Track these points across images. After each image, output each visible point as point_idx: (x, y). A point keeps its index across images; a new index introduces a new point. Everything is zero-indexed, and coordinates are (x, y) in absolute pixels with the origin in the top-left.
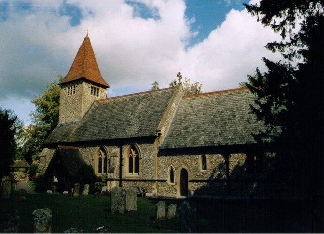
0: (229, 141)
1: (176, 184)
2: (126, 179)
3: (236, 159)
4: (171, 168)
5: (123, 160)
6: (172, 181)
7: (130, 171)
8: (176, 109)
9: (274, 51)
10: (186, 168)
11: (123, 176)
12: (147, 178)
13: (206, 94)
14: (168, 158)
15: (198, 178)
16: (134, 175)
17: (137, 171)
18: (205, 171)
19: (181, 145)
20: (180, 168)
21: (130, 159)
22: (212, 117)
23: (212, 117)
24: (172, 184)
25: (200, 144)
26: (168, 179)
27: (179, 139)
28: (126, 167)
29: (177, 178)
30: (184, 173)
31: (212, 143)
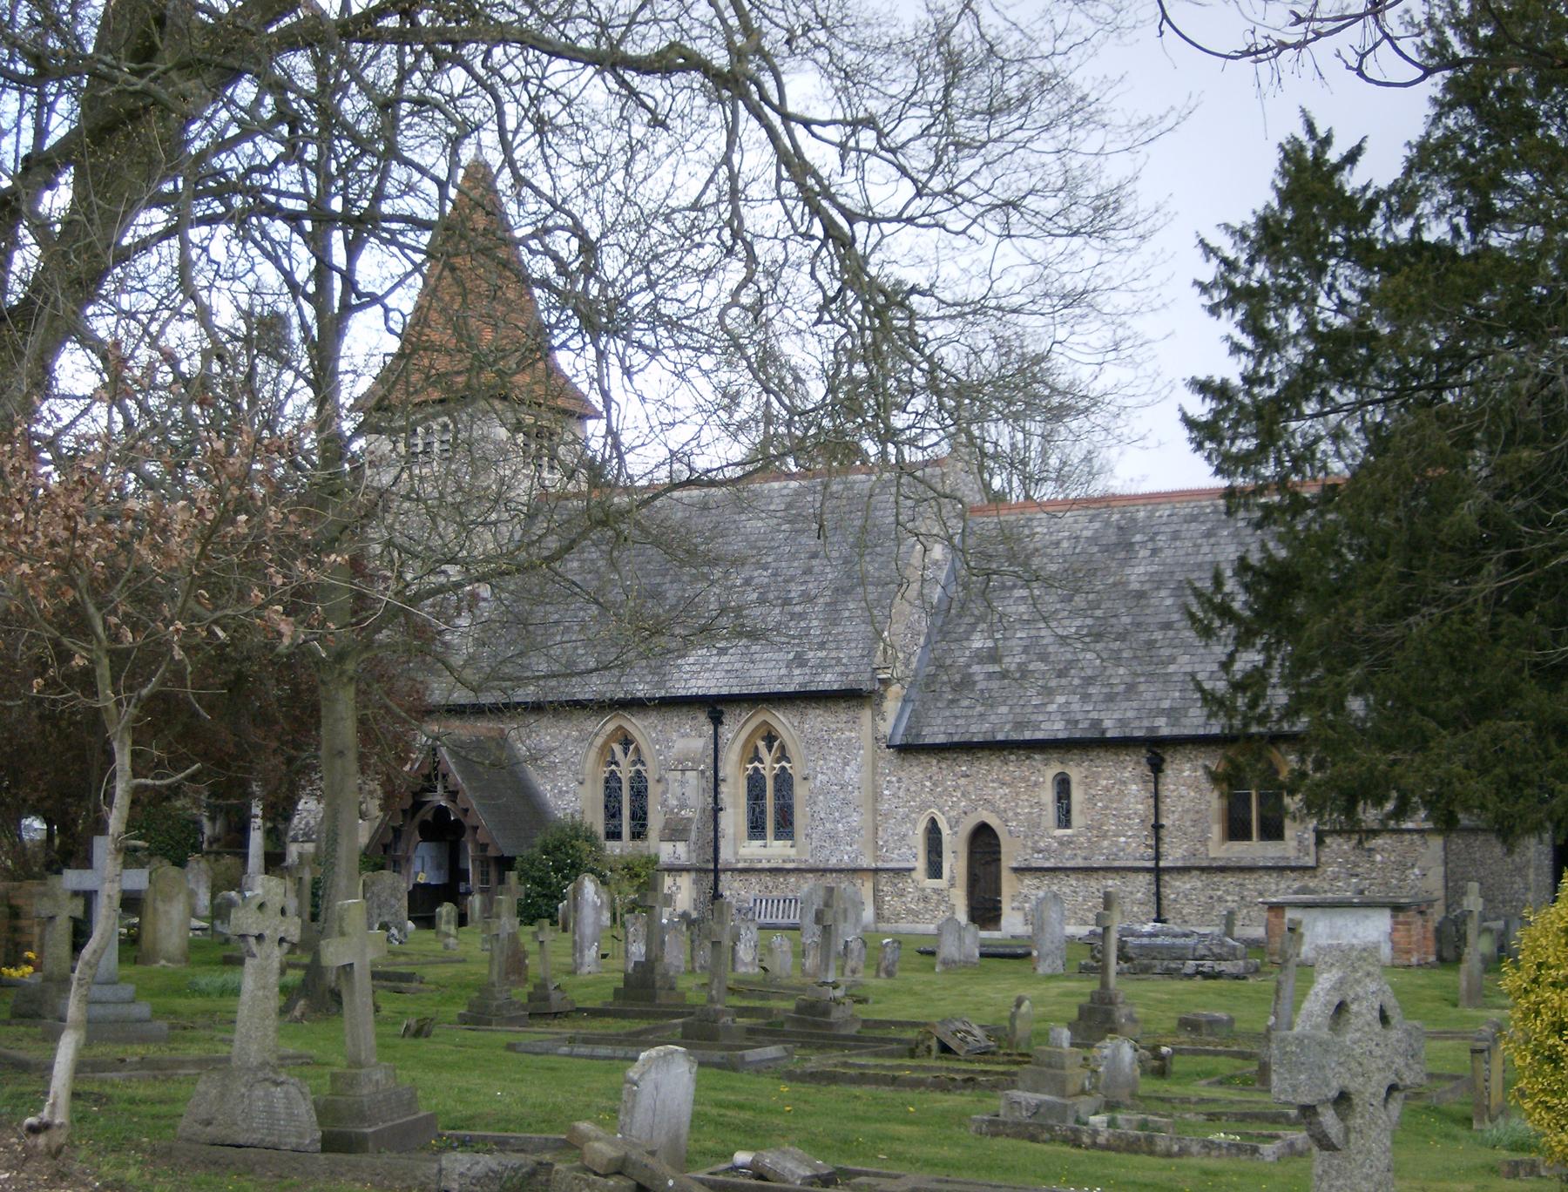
0: (1161, 722)
1: (952, 885)
2: (740, 865)
3: (785, 174)
4: (933, 821)
5: (721, 814)
6: (935, 870)
7: (756, 829)
8: (946, 568)
9: (1208, 260)
10: (994, 822)
11: (726, 854)
12: (833, 862)
13: (1382, 905)
14: (919, 772)
15: (1038, 861)
16: (774, 850)
17: (785, 827)
18: (1069, 831)
19: (973, 729)
20: (969, 824)
21: (755, 786)
22: (1099, 613)
23: (1099, 613)
24: (935, 883)
25: (1055, 728)
26: (920, 864)
27: (966, 703)
28: (734, 819)
29: (955, 862)
30: (984, 841)
31: (1096, 723)
